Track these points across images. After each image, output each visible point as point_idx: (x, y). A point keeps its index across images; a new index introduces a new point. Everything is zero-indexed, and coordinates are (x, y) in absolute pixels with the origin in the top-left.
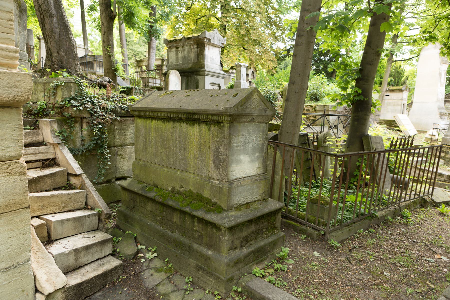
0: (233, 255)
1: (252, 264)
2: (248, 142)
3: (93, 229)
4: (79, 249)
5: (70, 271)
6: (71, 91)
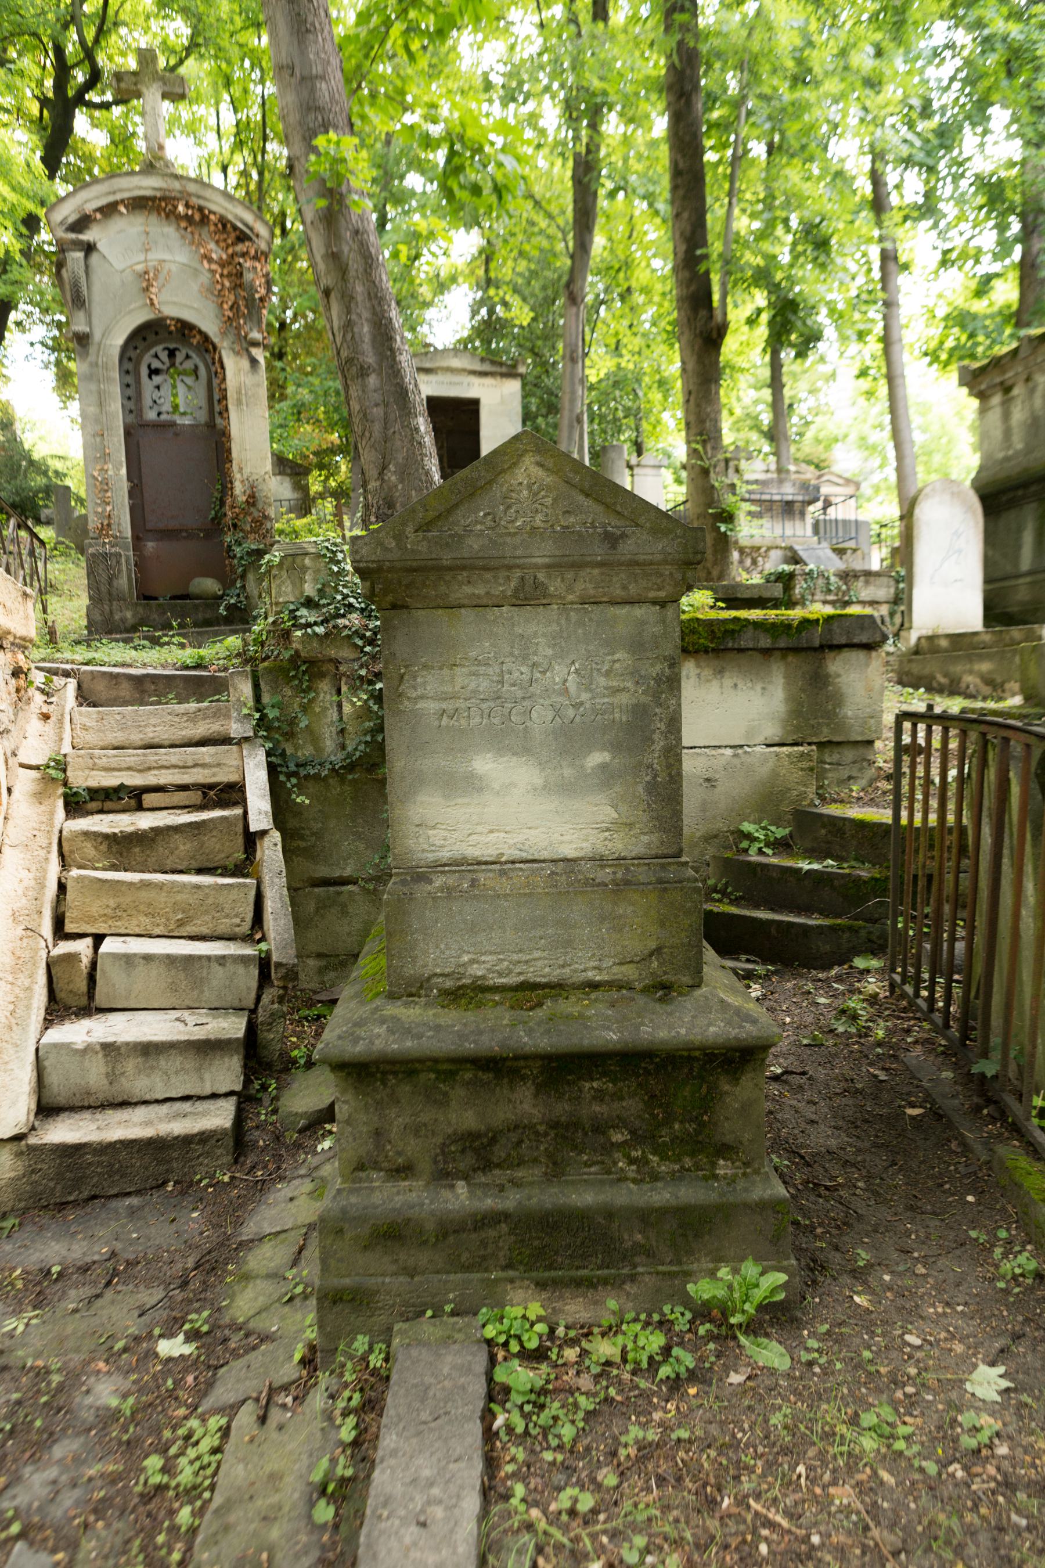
0: (377, 1198)
1: (501, 1274)
2: (520, 694)
3: (236, 1004)
4: (118, 1048)
5: (89, 1107)
6: (302, 581)
